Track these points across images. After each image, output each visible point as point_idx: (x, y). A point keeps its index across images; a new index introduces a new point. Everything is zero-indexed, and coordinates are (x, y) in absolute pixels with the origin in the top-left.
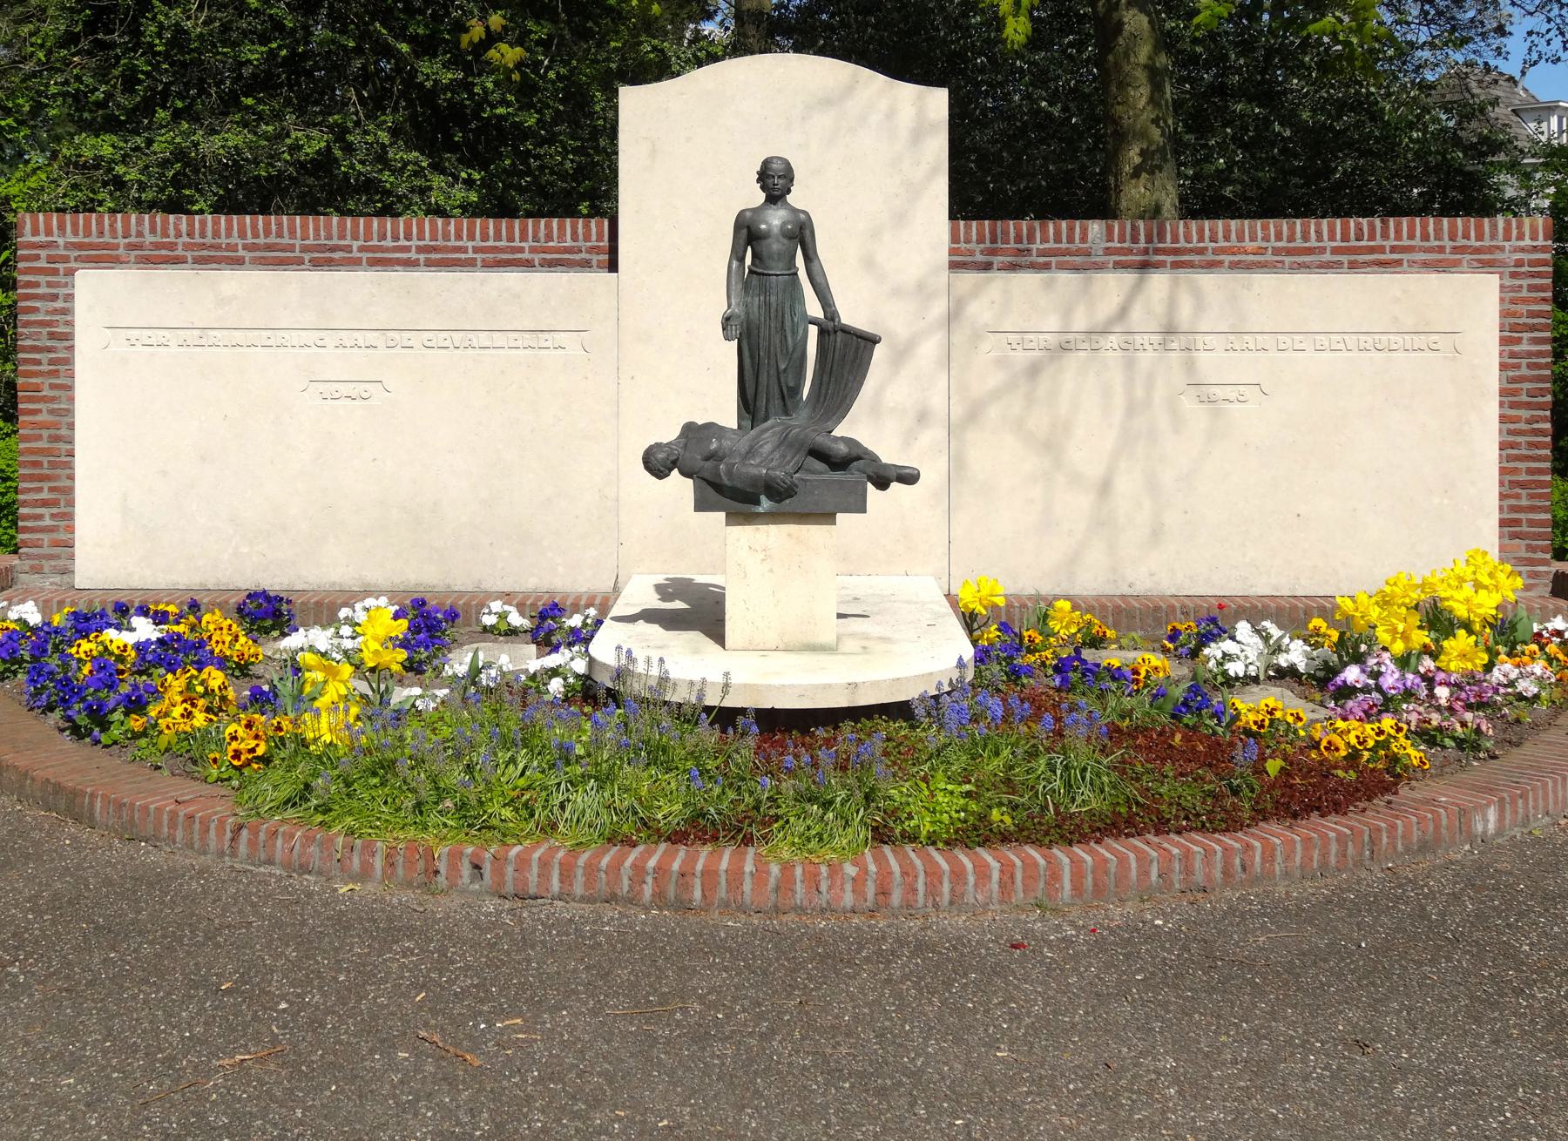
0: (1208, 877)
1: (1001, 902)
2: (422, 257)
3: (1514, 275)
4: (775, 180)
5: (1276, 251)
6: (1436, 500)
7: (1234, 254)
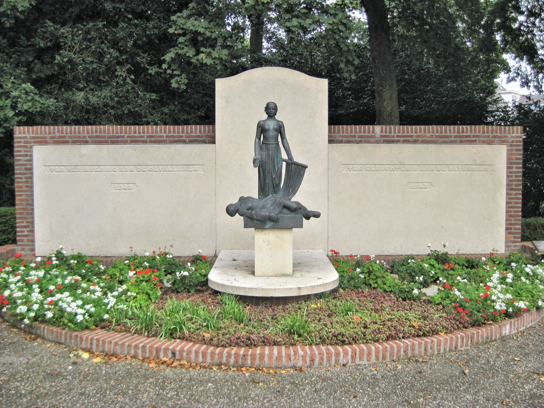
0: (420, 352)
1: (352, 362)
2: (148, 139)
3: (511, 146)
4: (271, 110)
5: (436, 137)
6: (486, 222)
7: (422, 137)
